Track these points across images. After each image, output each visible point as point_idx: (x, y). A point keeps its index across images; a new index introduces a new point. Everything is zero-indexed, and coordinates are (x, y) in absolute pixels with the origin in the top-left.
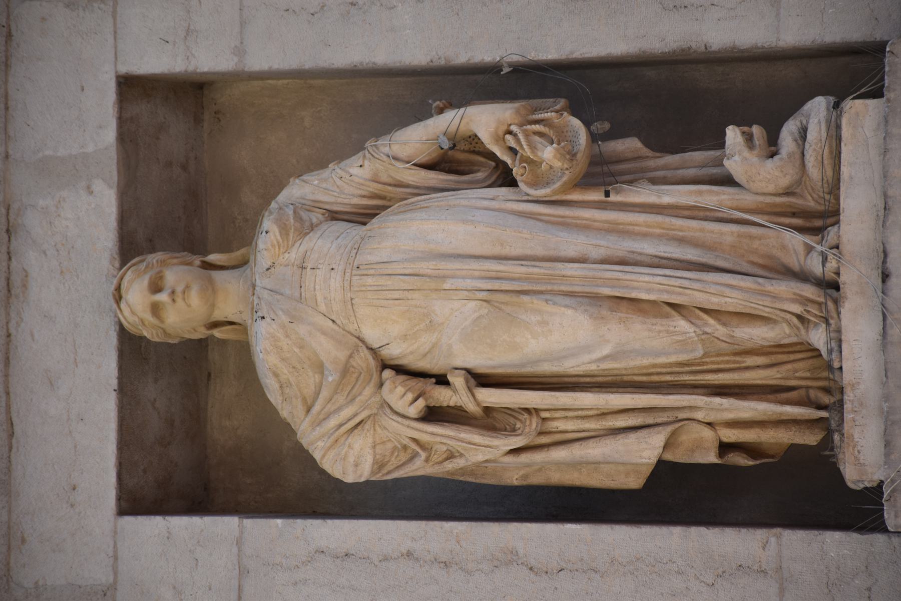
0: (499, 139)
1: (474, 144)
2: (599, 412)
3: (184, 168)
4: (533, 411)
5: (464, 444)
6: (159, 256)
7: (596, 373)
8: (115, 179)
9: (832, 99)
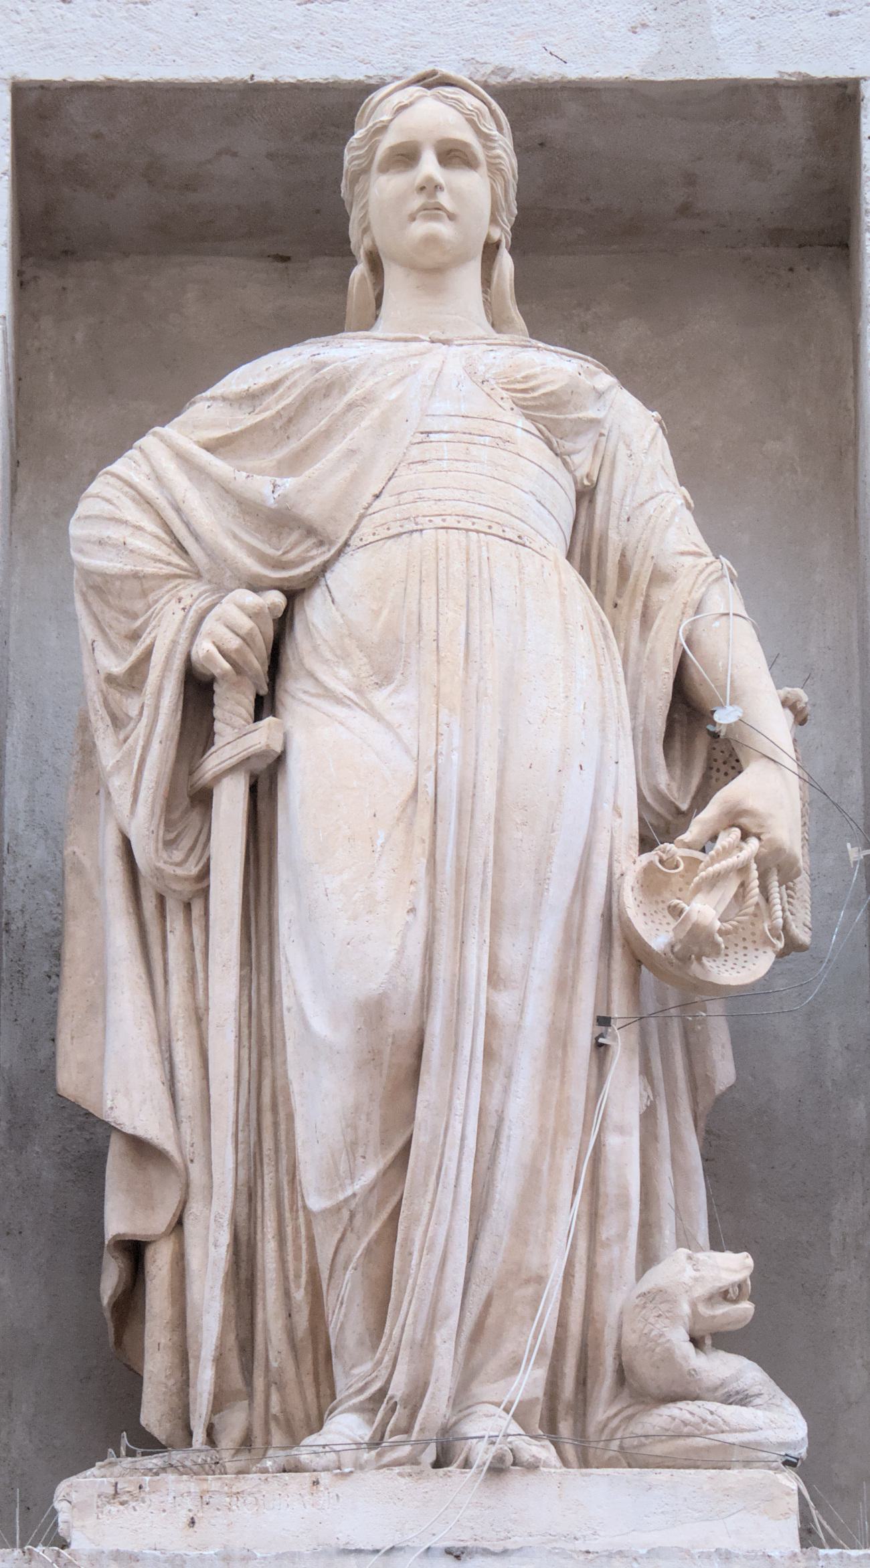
0: (735, 818)
1: (723, 768)
2: (201, 1011)
3: (685, 210)
4: (204, 885)
5: (139, 752)
6: (509, 160)
7: (277, 1008)
8: (660, 78)
9: (802, 1452)
